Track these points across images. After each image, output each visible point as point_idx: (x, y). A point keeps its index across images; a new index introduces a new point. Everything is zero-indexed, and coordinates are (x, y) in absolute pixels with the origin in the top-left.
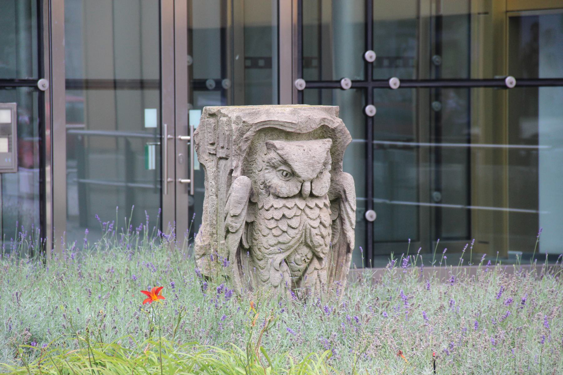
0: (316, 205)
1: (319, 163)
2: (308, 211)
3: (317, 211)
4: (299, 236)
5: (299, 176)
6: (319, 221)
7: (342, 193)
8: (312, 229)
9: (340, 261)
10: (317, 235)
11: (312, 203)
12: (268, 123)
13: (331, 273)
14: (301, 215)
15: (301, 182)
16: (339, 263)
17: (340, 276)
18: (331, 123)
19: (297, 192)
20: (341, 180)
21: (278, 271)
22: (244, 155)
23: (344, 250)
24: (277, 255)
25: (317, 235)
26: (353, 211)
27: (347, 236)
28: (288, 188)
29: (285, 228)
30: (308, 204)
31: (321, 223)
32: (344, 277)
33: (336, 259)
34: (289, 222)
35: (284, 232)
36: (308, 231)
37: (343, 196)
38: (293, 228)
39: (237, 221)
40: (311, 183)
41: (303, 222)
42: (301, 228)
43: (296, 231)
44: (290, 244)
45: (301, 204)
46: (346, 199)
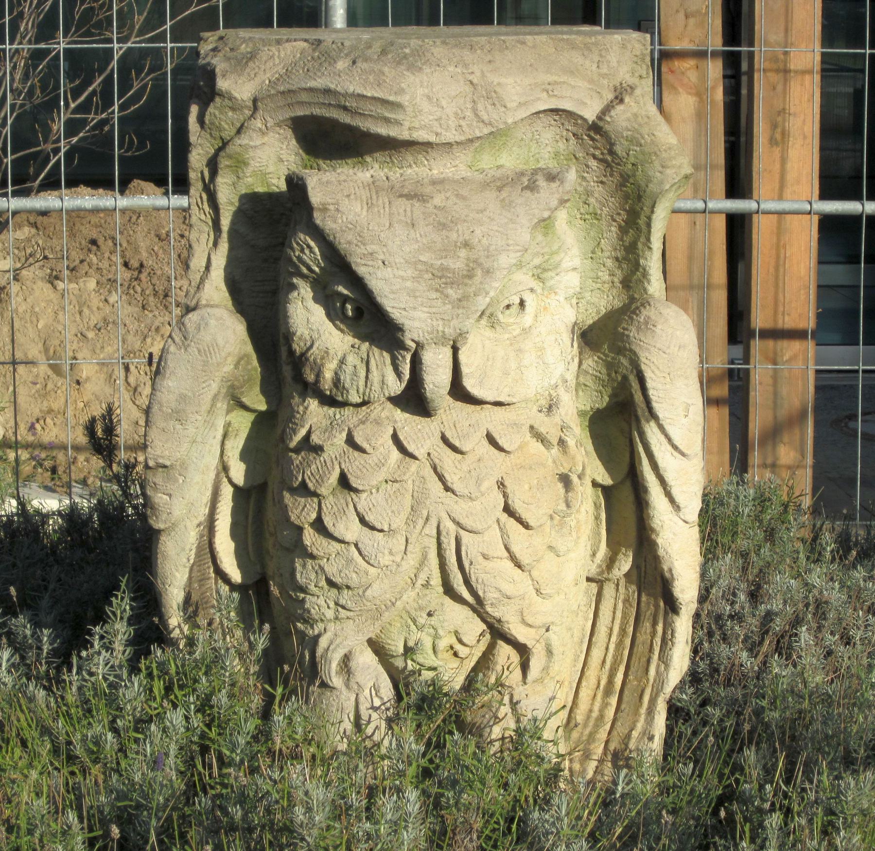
46: (652, 415)
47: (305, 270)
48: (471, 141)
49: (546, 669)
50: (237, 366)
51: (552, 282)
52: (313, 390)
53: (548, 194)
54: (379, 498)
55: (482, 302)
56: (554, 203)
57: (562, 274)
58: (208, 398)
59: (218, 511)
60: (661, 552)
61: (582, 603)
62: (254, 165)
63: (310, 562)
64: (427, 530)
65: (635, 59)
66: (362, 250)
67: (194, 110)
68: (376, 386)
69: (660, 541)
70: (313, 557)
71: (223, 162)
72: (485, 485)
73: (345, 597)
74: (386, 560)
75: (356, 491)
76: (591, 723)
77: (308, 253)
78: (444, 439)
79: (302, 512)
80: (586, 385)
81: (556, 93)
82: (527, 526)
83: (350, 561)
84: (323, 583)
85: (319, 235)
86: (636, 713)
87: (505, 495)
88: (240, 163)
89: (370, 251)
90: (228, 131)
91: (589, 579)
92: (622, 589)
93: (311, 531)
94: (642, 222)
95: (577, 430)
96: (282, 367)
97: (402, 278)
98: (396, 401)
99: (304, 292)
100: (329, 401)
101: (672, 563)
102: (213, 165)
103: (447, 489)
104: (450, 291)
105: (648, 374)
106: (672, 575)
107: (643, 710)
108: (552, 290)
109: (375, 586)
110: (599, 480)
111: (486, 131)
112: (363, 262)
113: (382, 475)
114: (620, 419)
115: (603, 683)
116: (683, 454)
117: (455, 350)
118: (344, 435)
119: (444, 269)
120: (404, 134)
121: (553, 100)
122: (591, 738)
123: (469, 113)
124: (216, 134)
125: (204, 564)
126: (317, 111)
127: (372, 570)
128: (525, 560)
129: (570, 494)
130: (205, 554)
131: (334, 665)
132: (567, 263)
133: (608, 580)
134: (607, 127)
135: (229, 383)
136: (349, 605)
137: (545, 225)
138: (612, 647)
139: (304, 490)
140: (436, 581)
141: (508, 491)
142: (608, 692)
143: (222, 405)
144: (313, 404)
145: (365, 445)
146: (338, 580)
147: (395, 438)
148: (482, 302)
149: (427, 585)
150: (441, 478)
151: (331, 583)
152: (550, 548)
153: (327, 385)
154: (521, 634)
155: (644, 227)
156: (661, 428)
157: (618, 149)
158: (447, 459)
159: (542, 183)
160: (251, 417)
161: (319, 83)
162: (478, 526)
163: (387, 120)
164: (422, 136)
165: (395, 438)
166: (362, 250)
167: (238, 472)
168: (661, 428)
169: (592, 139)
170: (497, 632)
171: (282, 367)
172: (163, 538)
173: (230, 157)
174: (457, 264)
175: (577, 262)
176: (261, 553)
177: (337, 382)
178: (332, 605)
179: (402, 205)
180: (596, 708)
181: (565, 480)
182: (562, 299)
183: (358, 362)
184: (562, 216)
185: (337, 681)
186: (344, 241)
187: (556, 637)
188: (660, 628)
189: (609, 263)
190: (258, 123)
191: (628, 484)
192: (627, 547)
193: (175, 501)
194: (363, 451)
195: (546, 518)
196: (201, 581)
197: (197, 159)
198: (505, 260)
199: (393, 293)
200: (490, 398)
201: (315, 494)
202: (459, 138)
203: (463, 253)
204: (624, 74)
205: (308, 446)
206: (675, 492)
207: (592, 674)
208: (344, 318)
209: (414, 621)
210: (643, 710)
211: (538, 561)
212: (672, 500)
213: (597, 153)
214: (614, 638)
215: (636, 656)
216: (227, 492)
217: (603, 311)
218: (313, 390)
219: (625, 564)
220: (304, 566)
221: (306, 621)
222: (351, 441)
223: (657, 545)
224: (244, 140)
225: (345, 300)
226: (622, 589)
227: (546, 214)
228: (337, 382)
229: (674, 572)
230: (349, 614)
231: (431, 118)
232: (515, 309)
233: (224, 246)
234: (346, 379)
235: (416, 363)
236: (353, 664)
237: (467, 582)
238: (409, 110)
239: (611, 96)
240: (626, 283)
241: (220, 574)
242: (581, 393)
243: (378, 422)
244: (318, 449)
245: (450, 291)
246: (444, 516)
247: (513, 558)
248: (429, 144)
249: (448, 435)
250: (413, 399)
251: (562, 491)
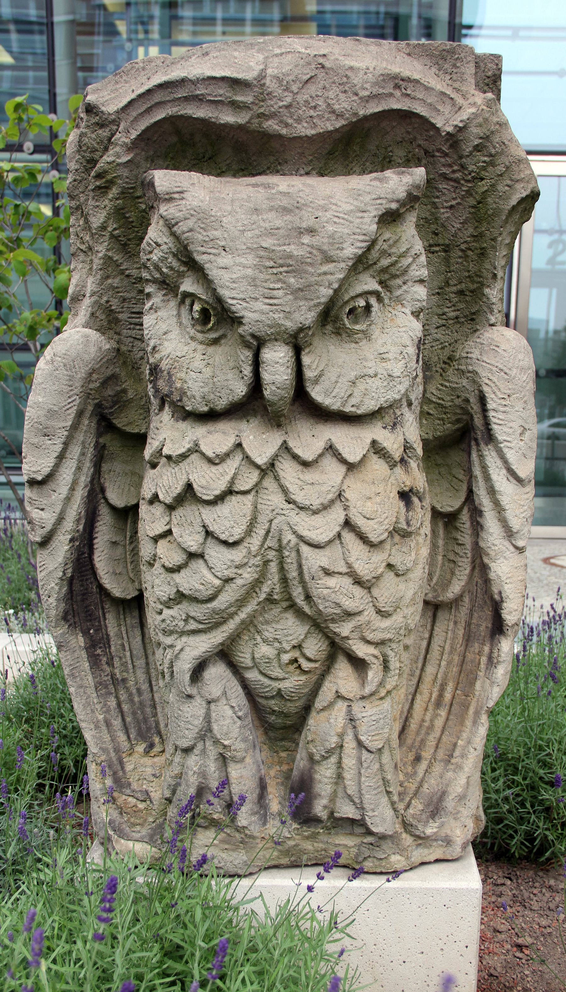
0: (331, 449)
1: (328, 259)
2: (288, 471)
3: (332, 474)
4: (249, 575)
5: (237, 321)
6: (337, 516)
7: (475, 407)
8: (305, 549)
9: (469, 656)
10: (328, 573)
11: (310, 439)
12: (158, 97)
13: (441, 695)
14: (257, 488)
15: (247, 345)
16: (468, 666)
17: (467, 707)
18: (446, 109)
19: (240, 389)
20: (475, 354)
21: (190, 697)
22: (102, 249)
23: (484, 625)
24: (184, 639)
25: (328, 573)
26: (519, 481)
27: (492, 575)
28: (208, 372)
29: (193, 542)
30: (291, 444)
31: (347, 524)
32: (477, 714)
33: (460, 649)
34: (209, 515)
35: (192, 556)
36: (290, 558)
37: (478, 421)
38: (225, 543)
39: (44, 502)
40: (298, 351)
41: (263, 519)
42: (255, 542)
43: (237, 555)
44: (221, 602)
45: (261, 443)
46: (490, 437)
51: (399, 292)
57: (410, 284)
59: (97, 530)
61: (199, 53)
65: (487, 81)
80: (428, 414)
81: (409, 92)
89: (212, 237)
101: (502, 586)
106: (502, 598)
108: (399, 300)
112: (203, 249)
115: (434, 695)
121: (406, 100)
125: (87, 580)
129: (410, 513)
130: (87, 570)
135: (96, 401)
142: (438, 704)
154: (361, 650)
175: (424, 273)
180: (428, 717)
182: (408, 311)
187: (393, 654)
196: (84, 594)
199: (234, 282)
207: (425, 687)
211: (377, 578)
223: (490, 568)
229: (503, 595)
231: (281, 104)
242: (424, 422)
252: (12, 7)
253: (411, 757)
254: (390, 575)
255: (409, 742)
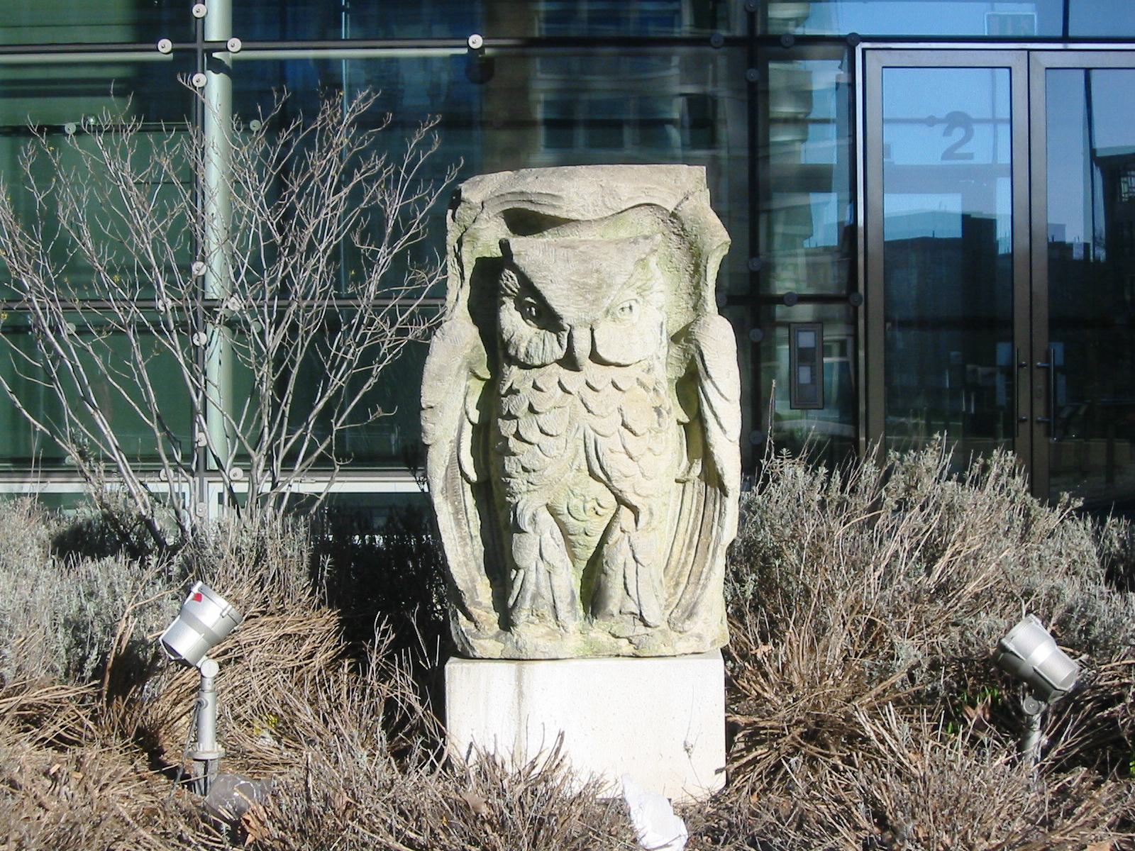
13: (691, 541)
46: (709, 377)
47: (509, 291)
48: (602, 219)
49: (648, 523)
50: (472, 351)
52: (513, 361)
53: (645, 246)
54: (549, 417)
55: (606, 303)
56: (647, 250)
58: (456, 366)
60: (716, 458)
62: (482, 239)
63: (512, 458)
64: (578, 436)
66: (539, 275)
67: (450, 212)
68: (549, 354)
69: (715, 452)
70: (514, 454)
71: (465, 239)
72: (611, 409)
73: (532, 477)
74: (555, 453)
75: (537, 413)
76: (680, 566)
77: (510, 281)
78: (587, 383)
79: (507, 428)
82: (635, 434)
83: (534, 454)
84: (520, 469)
85: (515, 269)
86: (706, 558)
87: (622, 416)
88: (475, 239)
90: (468, 222)
91: (677, 481)
92: (696, 486)
93: (514, 439)
94: (702, 269)
95: (666, 385)
96: (498, 351)
97: (562, 289)
98: (559, 362)
99: (509, 304)
100: (524, 366)
102: (460, 242)
103: (589, 411)
104: (588, 296)
105: (705, 352)
107: (710, 556)
109: (549, 469)
110: (681, 420)
111: (610, 213)
113: (551, 404)
114: (690, 386)
115: (687, 542)
116: (726, 399)
117: (592, 330)
118: (531, 383)
119: (585, 284)
120: (564, 215)
122: (680, 574)
123: (600, 203)
124: (462, 223)
126: (516, 205)
127: (547, 459)
128: (634, 454)
131: (527, 518)
132: (656, 288)
133: (688, 480)
134: (679, 214)
136: (535, 481)
137: (642, 262)
138: (691, 520)
139: (510, 416)
140: (584, 467)
141: (624, 413)
142: (689, 548)
143: (464, 373)
144: (514, 369)
145: (542, 387)
146: (527, 466)
147: (560, 383)
148: (606, 303)
149: (579, 470)
150: (585, 405)
151: (525, 470)
152: (650, 449)
153: (521, 356)
154: (633, 500)
155: (703, 273)
156: (713, 383)
157: (686, 227)
158: (589, 395)
159: (641, 240)
160: (483, 383)
161: (517, 189)
162: (607, 433)
163: (554, 206)
164: (573, 216)
165: (560, 383)
166: (539, 275)
167: (475, 416)
168: (713, 383)
169: (672, 222)
170: (621, 501)
171: (498, 351)
172: (430, 449)
173: (469, 236)
174: (592, 281)
176: (487, 468)
177: (527, 354)
178: (525, 482)
179: (563, 251)
180: (683, 557)
181: (658, 410)
183: (538, 341)
184: (653, 260)
185: (528, 528)
186: (529, 271)
188: (718, 506)
189: (685, 297)
190: (484, 216)
191: (697, 421)
192: (698, 458)
193: (437, 427)
194: (541, 390)
195: (645, 430)
197: (451, 239)
198: (620, 280)
200: (613, 360)
201: (516, 418)
202: (596, 217)
203: (595, 275)
204: (690, 187)
205: (513, 391)
206: (722, 422)
207: (680, 537)
208: (532, 318)
209: (572, 492)
210: (710, 556)
211: (642, 455)
212: (719, 424)
213: (675, 230)
214: (692, 516)
215: (706, 524)
216: (468, 429)
217: (683, 325)
218: (513, 361)
219: (697, 469)
220: (509, 461)
221: (511, 495)
222: (535, 387)
224: (476, 226)
225: (531, 305)
226: (696, 486)
227: (643, 256)
228: (527, 354)
230: (535, 487)
232: (627, 310)
233: (467, 287)
234: (532, 351)
235: (570, 337)
236: (537, 519)
237: (602, 468)
238: (566, 200)
239: (682, 197)
240: (695, 308)
241: (463, 474)
243: (550, 375)
244: (516, 392)
245: (588, 296)
246: (587, 426)
247: (628, 453)
248: (578, 221)
249: (589, 381)
250: (569, 361)
251: (656, 416)
252: (809, 205)
253: (673, 583)
254: (649, 454)
255: (671, 573)
